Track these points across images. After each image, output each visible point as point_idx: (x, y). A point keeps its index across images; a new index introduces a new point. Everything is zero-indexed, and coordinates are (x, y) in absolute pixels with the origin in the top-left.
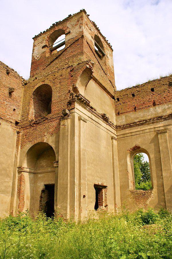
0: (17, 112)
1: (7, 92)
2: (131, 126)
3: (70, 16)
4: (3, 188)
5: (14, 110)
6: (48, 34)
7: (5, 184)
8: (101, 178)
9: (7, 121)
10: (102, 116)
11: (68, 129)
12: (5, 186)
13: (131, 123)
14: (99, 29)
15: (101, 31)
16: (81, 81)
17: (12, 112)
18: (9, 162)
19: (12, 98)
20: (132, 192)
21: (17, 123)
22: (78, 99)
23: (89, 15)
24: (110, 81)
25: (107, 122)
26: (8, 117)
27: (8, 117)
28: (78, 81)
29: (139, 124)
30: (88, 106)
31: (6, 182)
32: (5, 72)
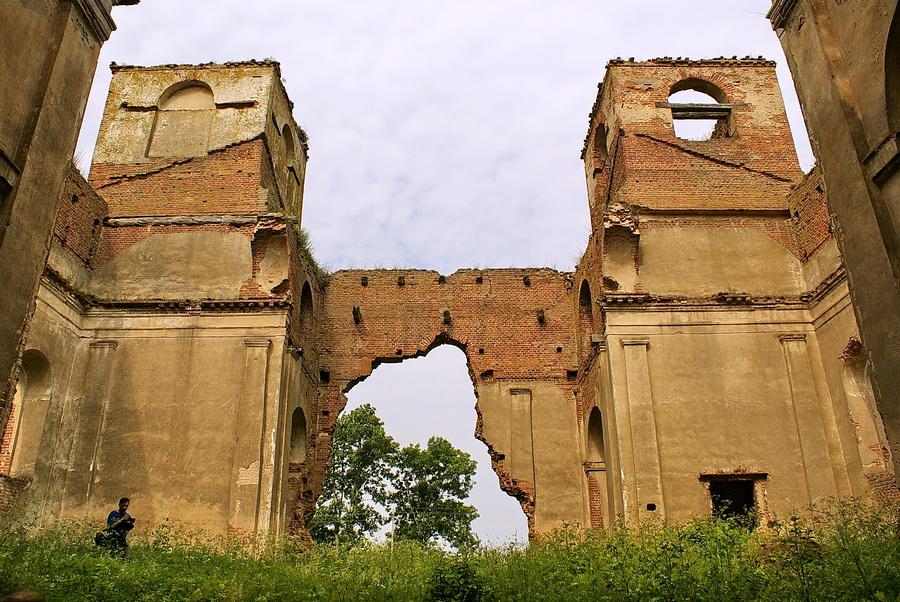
0: (566, 351)
1: (533, 321)
2: (829, 285)
3: (600, 85)
4: (563, 509)
5: (559, 350)
6: (591, 147)
7: (566, 501)
8: (728, 458)
9: (546, 379)
10: (717, 300)
11: (273, 510)
12: (567, 505)
13: (827, 279)
14: (683, 59)
15: (693, 58)
16: (612, 260)
17: (554, 356)
18: (569, 455)
19: (548, 327)
20: (871, 478)
21: (571, 375)
22: (609, 304)
23: (632, 60)
24: (763, 173)
25: (749, 304)
26: (548, 369)
27: (548, 369)
28: (605, 264)
29: (842, 275)
30: (650, 302)
31: (567, 496)
32: (521, 284)
